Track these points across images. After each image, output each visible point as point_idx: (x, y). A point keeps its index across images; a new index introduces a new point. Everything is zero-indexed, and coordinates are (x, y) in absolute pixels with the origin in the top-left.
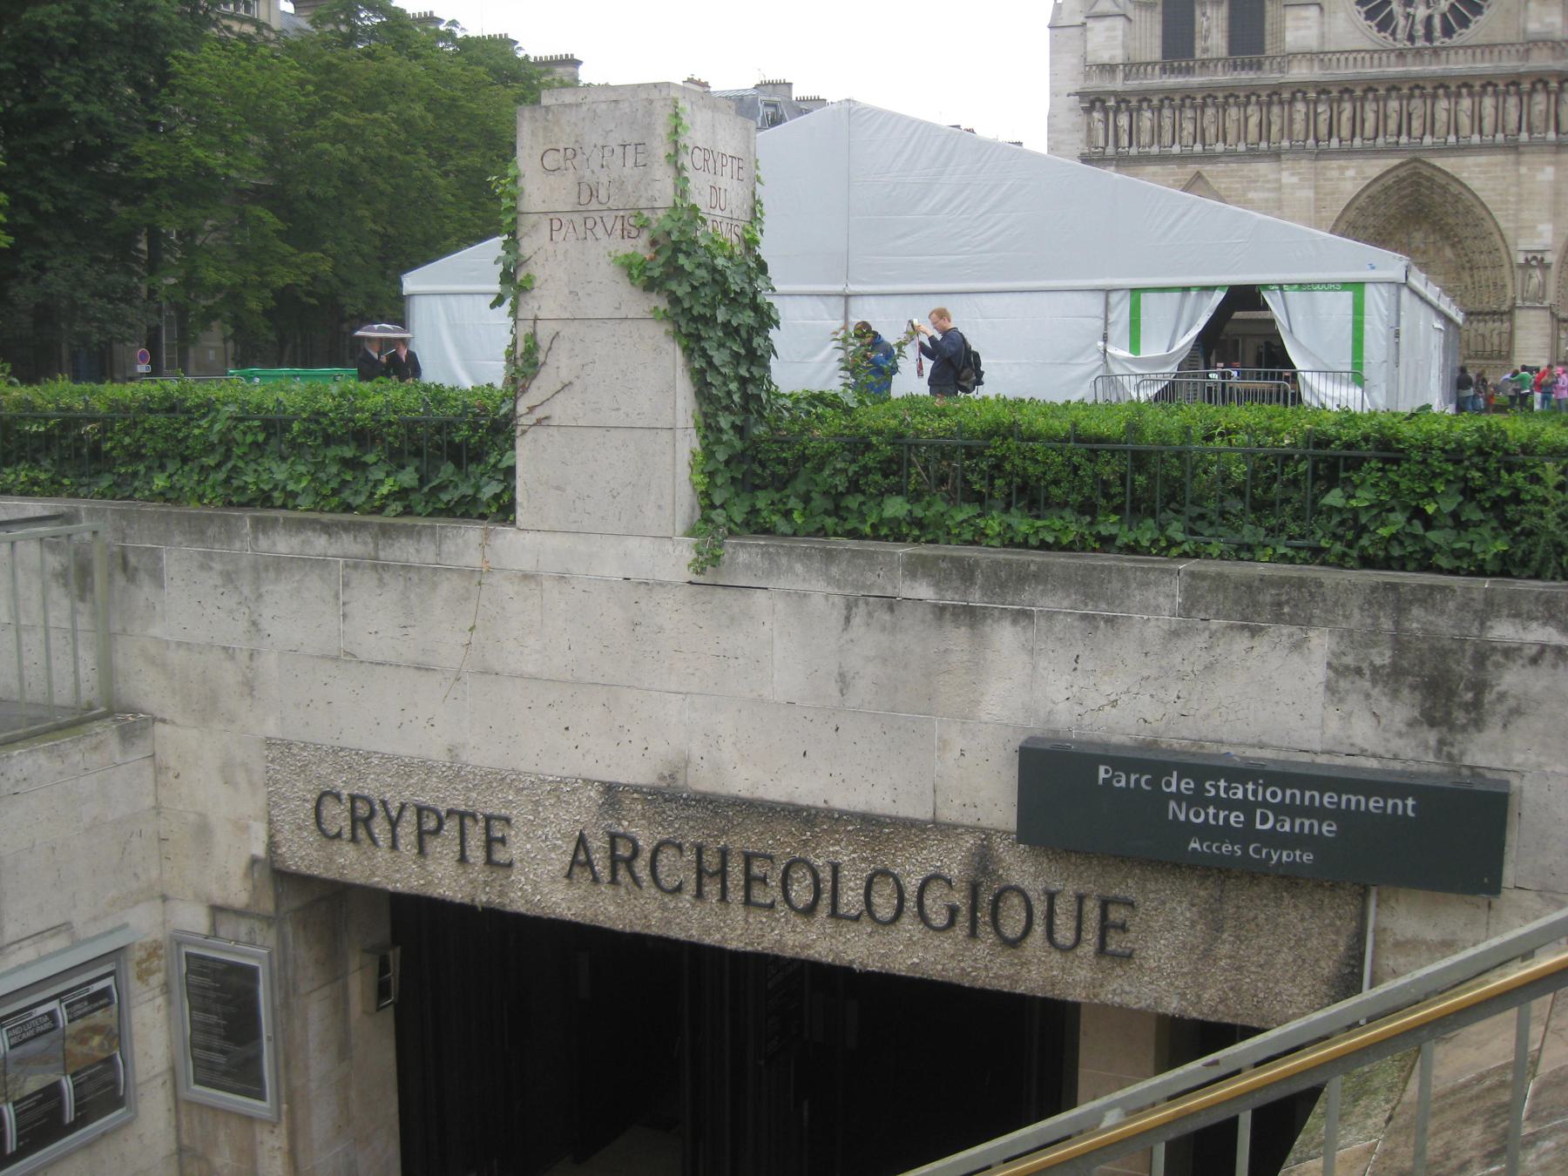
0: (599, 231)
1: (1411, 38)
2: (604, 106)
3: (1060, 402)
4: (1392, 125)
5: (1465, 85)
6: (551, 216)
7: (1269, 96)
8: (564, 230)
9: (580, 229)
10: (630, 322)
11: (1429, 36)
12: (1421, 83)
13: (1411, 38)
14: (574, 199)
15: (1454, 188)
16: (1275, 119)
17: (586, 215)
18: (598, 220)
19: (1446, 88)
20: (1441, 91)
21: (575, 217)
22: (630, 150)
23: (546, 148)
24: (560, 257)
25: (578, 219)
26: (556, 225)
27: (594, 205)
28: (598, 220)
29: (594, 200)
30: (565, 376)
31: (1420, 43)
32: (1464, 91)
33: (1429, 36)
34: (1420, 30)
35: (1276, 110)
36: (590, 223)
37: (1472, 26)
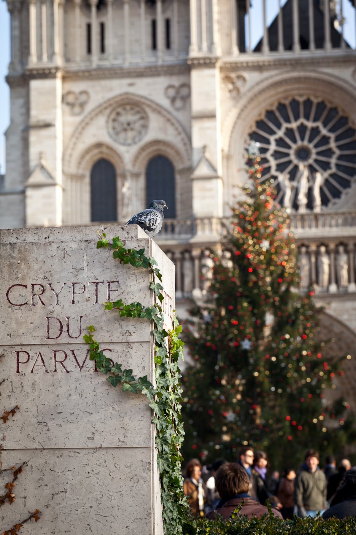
0: (70, 364)
1: (295, 206)
2: (74, 246)
3: (15, 524)
4: (325, 277)
5: (341, 244)
6: (18, 349)
7: (182, 253)
8: (32, 363)
9: (50, 363)
10: (104, 452)
11: (310, 205)
12: (306, 243)
13: (295, 206)
14: (43, 332)
15: (337, 329)
16: (188, 273)
17: (55, 348)
18: (69, 353)
19: (327, 246)
20: (341, 249)
21: (43, 350)
22: (103, 289)
23: (11, 284)
24: (28, 389)
25: (47, 353)
26: (23, 357)
27: (64, 339)
28: (69, 353)
29: (65, 334)
30: (32, 505)
31: (303, 210)
32: (341, 249)
33: (310, 205)
34: (303, 200)
35: (187, 265)
36: (60, 356)
37: (343, 197)
